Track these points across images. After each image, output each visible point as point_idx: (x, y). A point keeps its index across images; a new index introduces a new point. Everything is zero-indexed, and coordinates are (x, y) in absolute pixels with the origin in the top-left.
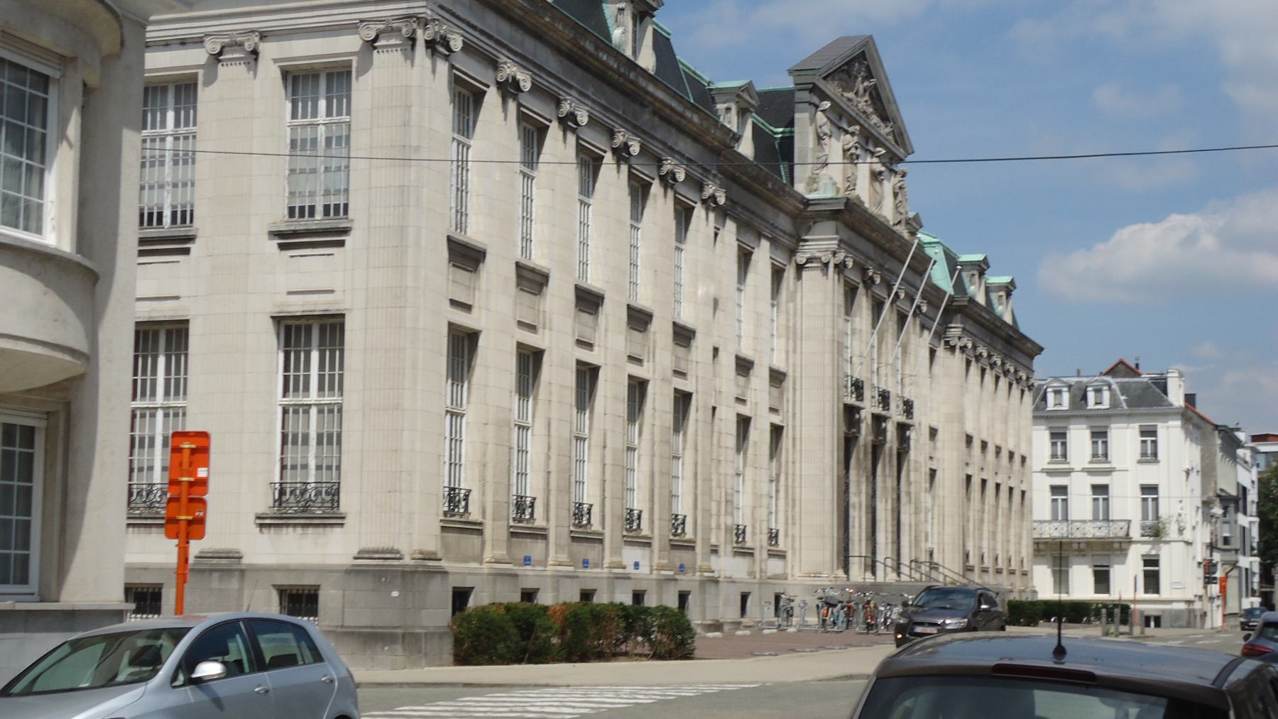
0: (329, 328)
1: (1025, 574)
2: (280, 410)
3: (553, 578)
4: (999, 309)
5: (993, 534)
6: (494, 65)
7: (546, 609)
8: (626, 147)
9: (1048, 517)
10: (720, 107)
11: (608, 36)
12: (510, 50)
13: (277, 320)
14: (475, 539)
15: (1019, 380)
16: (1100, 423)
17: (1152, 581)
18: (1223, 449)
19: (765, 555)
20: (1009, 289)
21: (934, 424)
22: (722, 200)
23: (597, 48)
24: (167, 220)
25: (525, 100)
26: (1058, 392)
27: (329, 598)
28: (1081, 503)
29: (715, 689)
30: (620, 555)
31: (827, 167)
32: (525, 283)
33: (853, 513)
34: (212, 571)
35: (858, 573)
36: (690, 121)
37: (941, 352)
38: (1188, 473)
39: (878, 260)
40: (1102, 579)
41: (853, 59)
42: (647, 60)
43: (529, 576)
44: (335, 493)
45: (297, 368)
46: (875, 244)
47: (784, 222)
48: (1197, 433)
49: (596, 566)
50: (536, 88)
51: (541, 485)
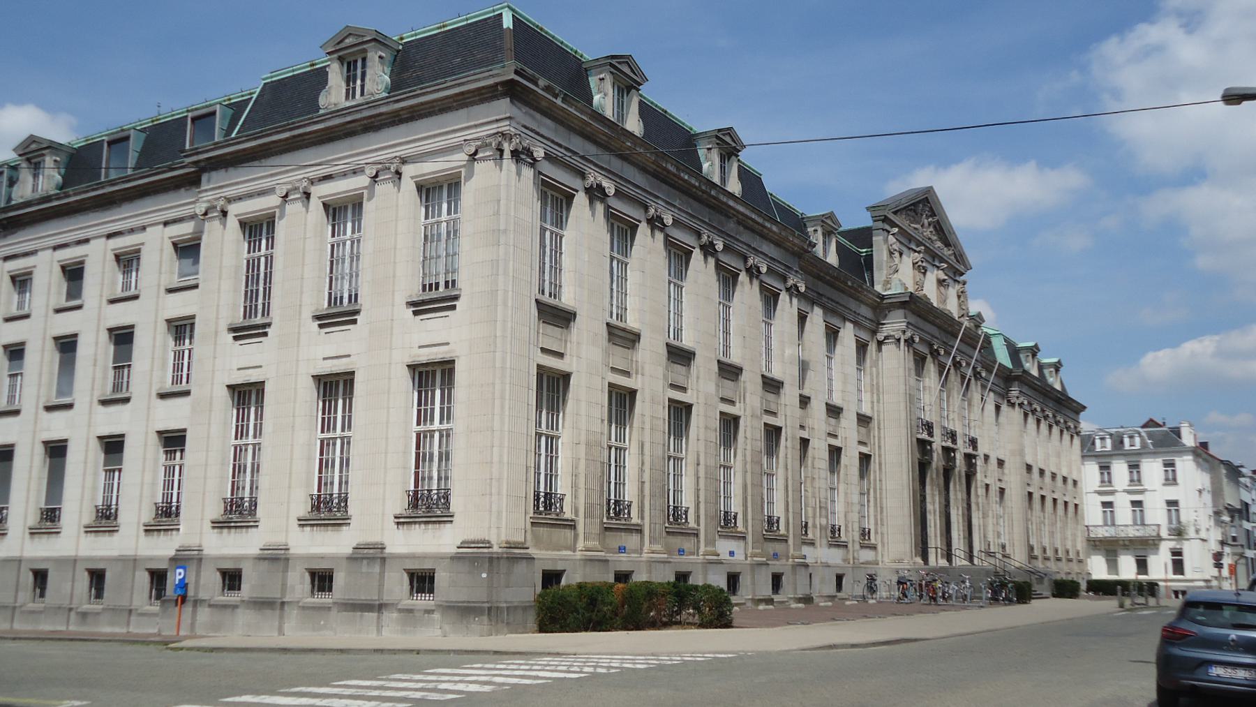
0: (446, 369)
1: (1080, 561)
2: (414, 435)
3: (648, 560)
4: (1051, 380)
5: (1052, 534)
6: (583, 176)
7: (696, 588)
8: (712, 245)
9: (1101, 523)
10: (810, 230)
11: (700, 168)
12: (596, 165)
13: (412, 367)
14: (568, 533)
15: (1068, 428)
16: (1134, 459)
17: (1178, 566)
18: (1228, 476)
19: (857, 546)
20: (1057, 367)
21: (1001, 457)
22: (802, 289)
23: (678, 169)
24: (346, 301)
25: (668, 231)
26: (1102, 439)
27: (441, 579)
28: (1124, 514)
29: (677, 659)
30: (714, 545)
31: (897, 273)
32: (618, 340)
33: (930, 517)
34: (363, 558)
35: (936, 560)
36: (770, 230)
37: (1004, 407)
38: (1200, 491)
39: (942, 341)
40: (1142, 565)
41: (919, 202)
42: (734, 186)
43: (623, 562)
44: (447, 497)
45: (426, 404)
46: (939, 327)
47: (865, 311)
48: (1206, 465)
49: (692, 554)
50: (619, 194)
51: (636, 492)
